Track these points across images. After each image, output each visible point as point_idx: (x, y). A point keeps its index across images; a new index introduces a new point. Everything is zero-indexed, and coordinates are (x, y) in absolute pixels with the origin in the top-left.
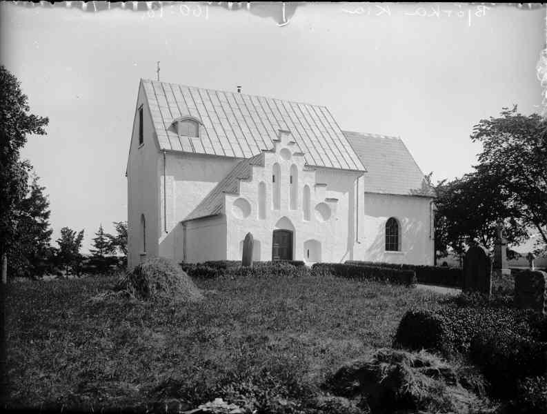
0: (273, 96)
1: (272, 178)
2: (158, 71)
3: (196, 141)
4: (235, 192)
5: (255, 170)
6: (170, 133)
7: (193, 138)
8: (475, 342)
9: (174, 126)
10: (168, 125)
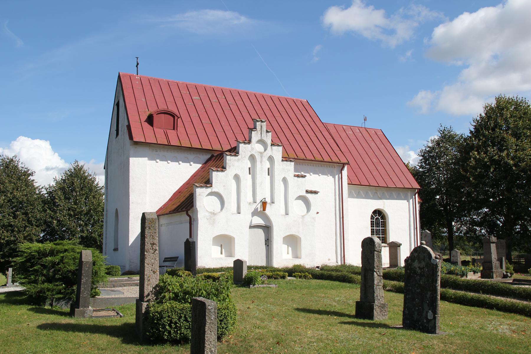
0: (254, 92)
1: (314, 190)
2: (138, 64)
3: (172, 134)
4: (208, 183)
5: (229, 159)
6: (146, 125)
7: (168, 131)
8: (395, 289)
9: (150, 120)
10: (144, 117)
